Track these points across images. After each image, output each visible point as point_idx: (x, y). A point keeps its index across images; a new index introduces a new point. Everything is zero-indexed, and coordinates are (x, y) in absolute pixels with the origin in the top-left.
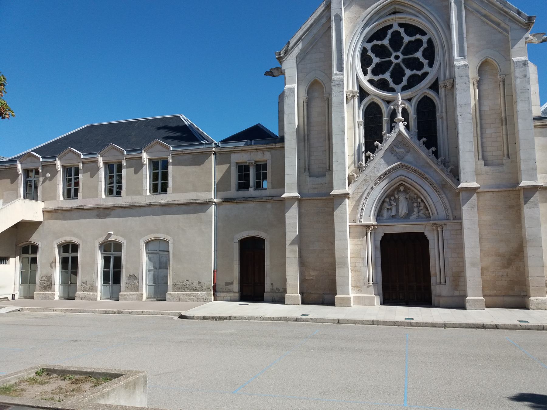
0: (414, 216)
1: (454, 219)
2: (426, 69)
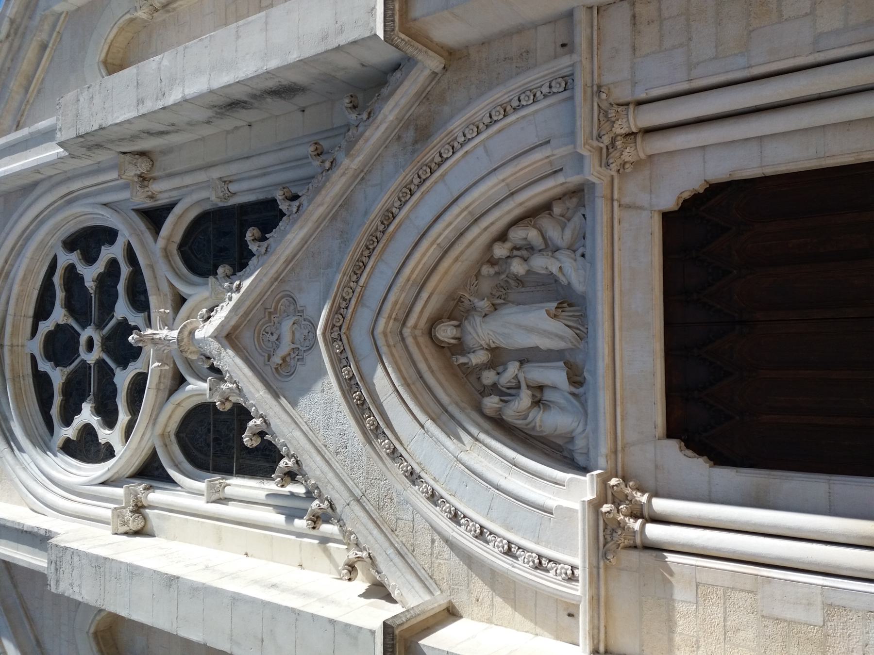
0: (569, 269)
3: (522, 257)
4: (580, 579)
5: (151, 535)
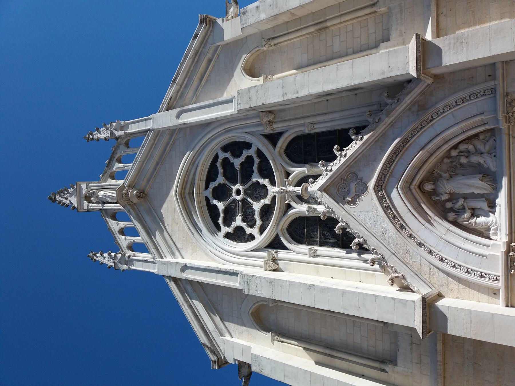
0: (490, 163)
1: (495, 79)
2: (252, 152)
3: (465, 156)
4: (500, 280)
5: (281, 271)
